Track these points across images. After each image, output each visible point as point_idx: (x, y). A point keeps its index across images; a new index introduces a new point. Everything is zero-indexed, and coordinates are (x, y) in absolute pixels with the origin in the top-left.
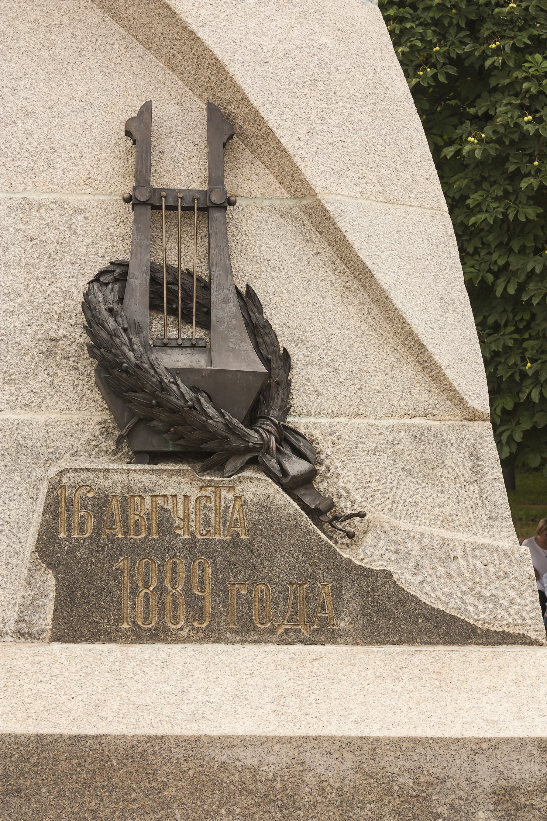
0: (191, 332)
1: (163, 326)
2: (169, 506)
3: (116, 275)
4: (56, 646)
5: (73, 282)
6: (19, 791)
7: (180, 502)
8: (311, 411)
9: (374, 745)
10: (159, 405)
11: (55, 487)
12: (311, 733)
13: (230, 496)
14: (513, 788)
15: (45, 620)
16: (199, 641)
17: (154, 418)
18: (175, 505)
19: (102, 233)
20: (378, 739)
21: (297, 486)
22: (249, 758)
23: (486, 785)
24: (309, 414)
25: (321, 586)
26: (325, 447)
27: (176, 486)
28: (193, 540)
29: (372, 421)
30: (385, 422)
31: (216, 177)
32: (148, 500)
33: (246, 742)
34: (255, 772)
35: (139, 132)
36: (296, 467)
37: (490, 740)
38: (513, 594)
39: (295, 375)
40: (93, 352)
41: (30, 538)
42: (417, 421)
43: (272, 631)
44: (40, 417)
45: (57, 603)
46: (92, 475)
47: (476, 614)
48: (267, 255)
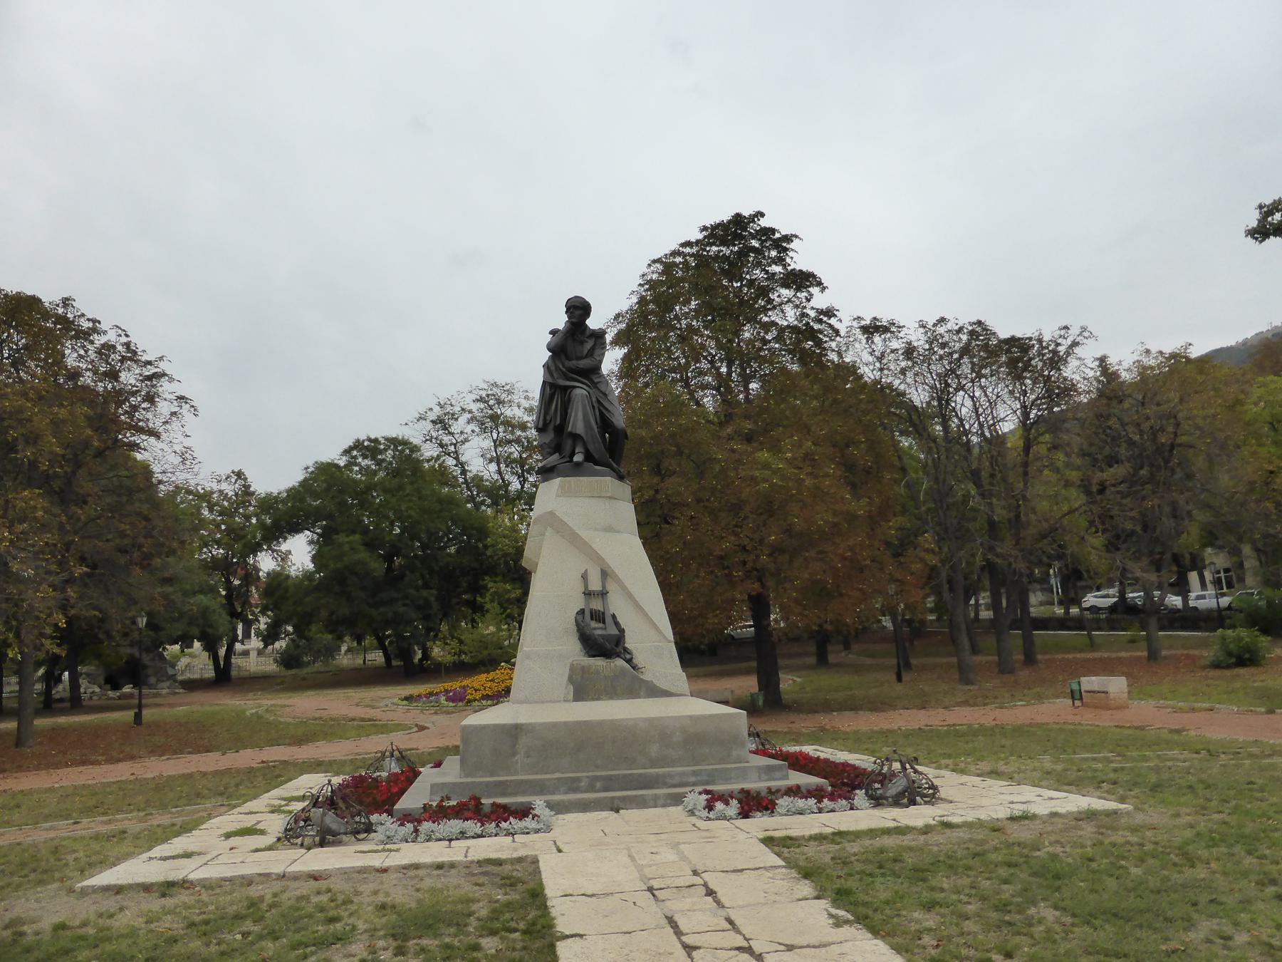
0: (601, 625)
1: (593, 624)
3: (582, 612)
8: (630, 643)
11: (572, 665)
15: (571, 696)
19: (578, 603)
21: (629, 661)
25: (635, 685)
26: (634, 652)
27: (599, 662)
31: (604, 586)
35: (584, 577)
36: (628, 656)
40: (901, 795)
41: (566, 678)
47: (673, 690)
48: (617, 605)
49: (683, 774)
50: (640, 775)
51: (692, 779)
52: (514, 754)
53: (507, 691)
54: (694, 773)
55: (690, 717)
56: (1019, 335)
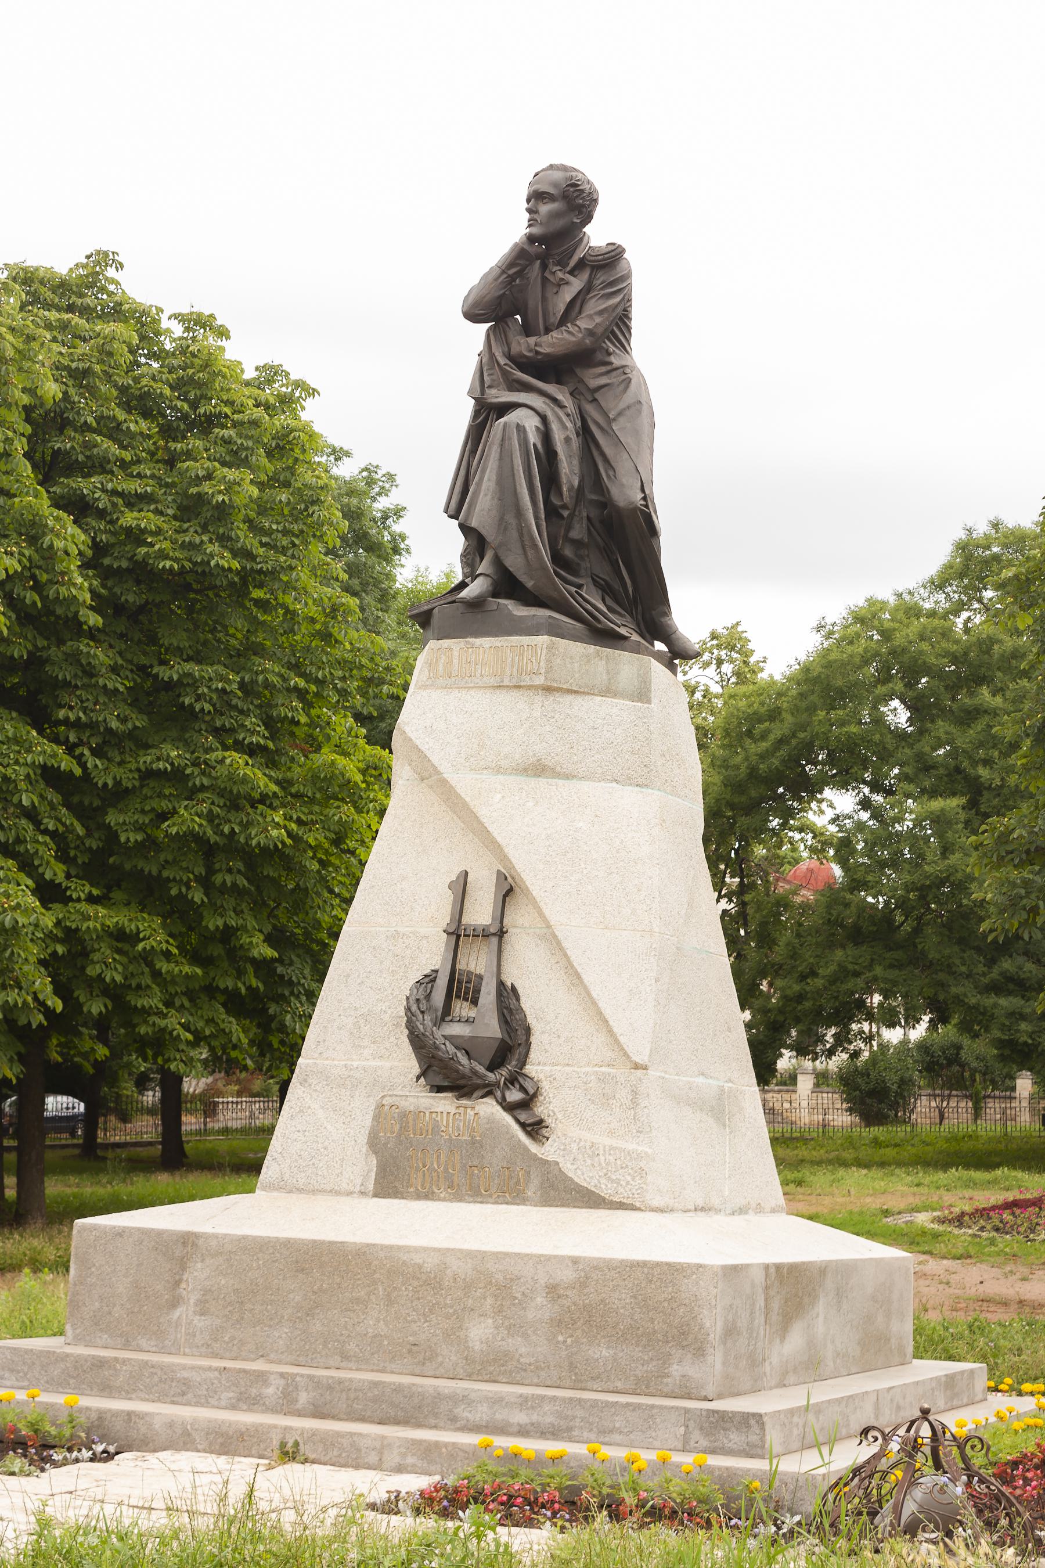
2: (439, 1119)
4: (375, 1200)
5: (405, 984)
6: (303, 1270)
7: (445, 1115)
9: (483, 1255)
10: (433, 1057)
12: (452, 1246)
13: (472, 1113)
14: (557, 1285)
15: (371, 1186)
16: (451, 1200)
17: (443, 1074)
18: (442, 1118)
19: (433, 955)
20: (485, 1252)
22: (418, 1259)
23: (542, 1282)
24: (539, 1064)
27: (445, 1104)
28: (450, 1140)
29: (576, 1069)
30: (584, 1070)
32: (427, 1114)
33: (416, 1250)
34: (420, 1267)
35: (461, 887)
37: (546, 1256)
38: (629, 1178)
39: (533, 1039)
42: (603, 1069)
43: (490, 1196)
44: (388, 1064)
45: (377, 1174)
46: (398, 1098)
47: (606, 1190)
49: (497, 1401)
50: (398, 1389)
51: (520, 1418)
52: (175, 1303)
53: (255, 1168)
54: (524, 1402)
55: (575, 1261)
56: (317, 428)
